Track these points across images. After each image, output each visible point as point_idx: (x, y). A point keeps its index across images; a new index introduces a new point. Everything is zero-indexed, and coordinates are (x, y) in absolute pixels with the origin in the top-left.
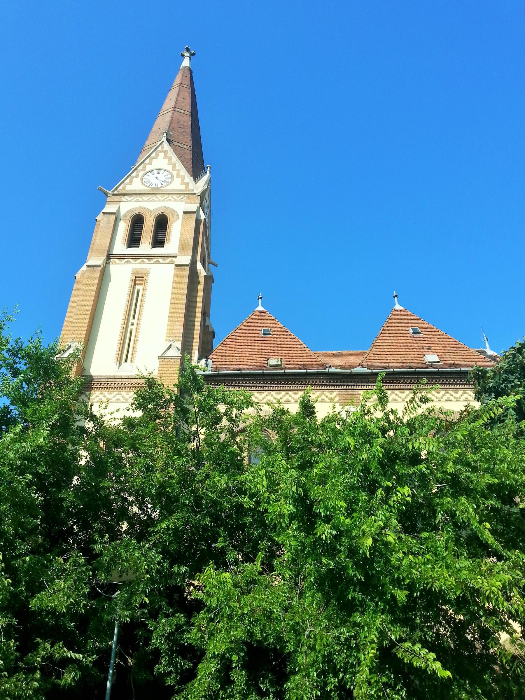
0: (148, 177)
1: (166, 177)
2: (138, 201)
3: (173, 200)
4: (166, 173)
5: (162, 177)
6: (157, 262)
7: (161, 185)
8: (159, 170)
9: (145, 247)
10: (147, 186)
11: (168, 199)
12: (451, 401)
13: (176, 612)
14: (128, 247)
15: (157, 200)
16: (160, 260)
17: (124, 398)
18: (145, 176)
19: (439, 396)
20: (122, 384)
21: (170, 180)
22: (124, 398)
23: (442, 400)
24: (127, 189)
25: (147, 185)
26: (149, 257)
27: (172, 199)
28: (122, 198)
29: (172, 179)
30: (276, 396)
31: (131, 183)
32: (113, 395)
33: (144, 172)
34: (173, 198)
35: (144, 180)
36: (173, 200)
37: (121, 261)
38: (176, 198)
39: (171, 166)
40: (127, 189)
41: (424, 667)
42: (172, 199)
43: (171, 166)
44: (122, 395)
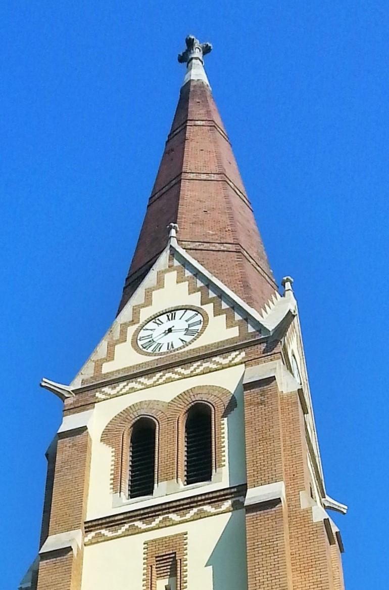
0: (149, 333)
1: (190, 322)
2: (133, 390)
4: (190, 313)
5: (180, 322)
8: (171, 313)
9: (170, 489)
10: (148, 354)
11: (127, 388)
13: (94, 376)
16: (207, 508)
18: (143, 333)
21: (199, 327)
25: (150, 350)
27: (173, 376)
28: (98, 394)
29: (205, 321)
31: (110, 356)
34: (176, 373)
35: (140, 343)
37: (116, 531)
38: (183, 371)
39: (198, 295)
42: (173, 376)
43: (198, 295)
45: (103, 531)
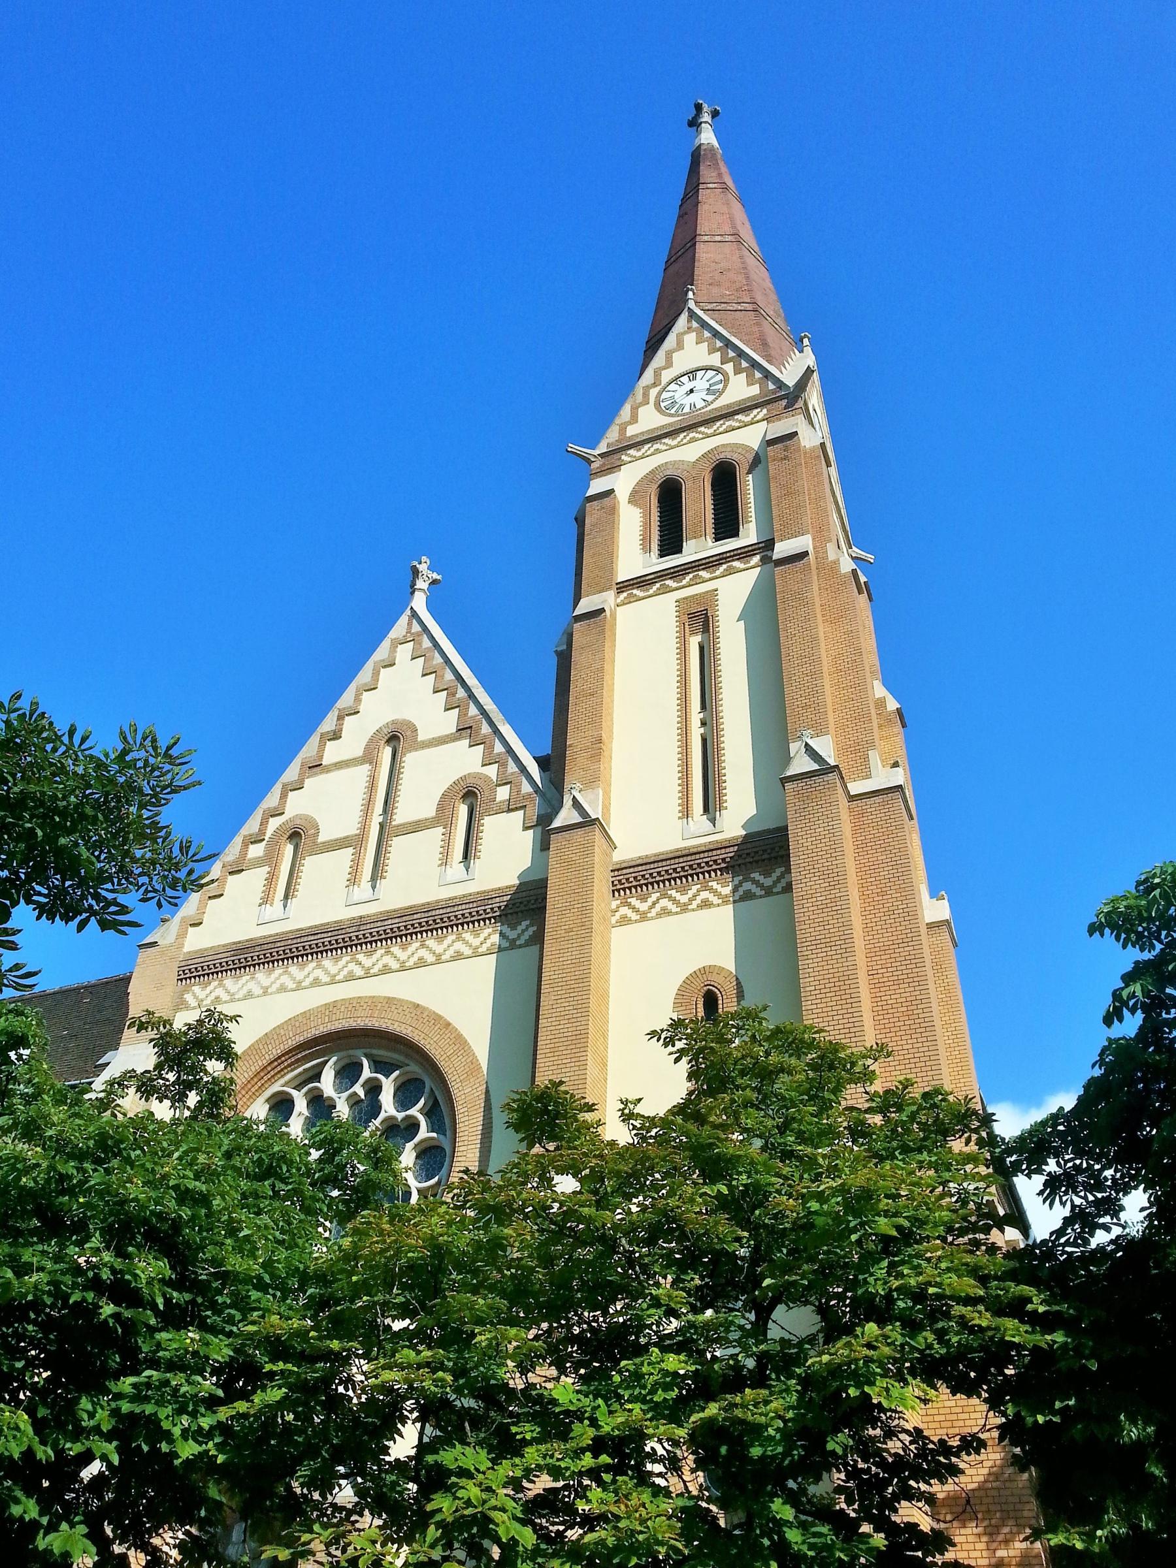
0: (671, 394)
2: (658, 451)
3: (665, 447)
4: (711, 373)
5: (701, 383)
6: (730, 572)
7: (703, 404)
8: (692, 373)
9: (697, 548)
12: (670, 913)
14: (661, 556)
15: (665, 447)
17: (761, 886)
18: (665, 395)
19: (768, 882)
20: (773, 849)
21: (721, 386)
22: (761, 886)
23: (518, 943)
24: (628, 434)
25: (673, 411)
26: (709, 564)
27: (697, 435)
29: (726, 380)
30: (761, 879)
31: (634, 419)
32: (775, 876)
33: (658, 388)
35: (662, 405)
36: (737, 424)
37: (648, 590)
38: (706, 430)
40: (628, 434)
41: (426, 1559)
42: (697, 435)
44: (754, 882)
45: (635, 591)
